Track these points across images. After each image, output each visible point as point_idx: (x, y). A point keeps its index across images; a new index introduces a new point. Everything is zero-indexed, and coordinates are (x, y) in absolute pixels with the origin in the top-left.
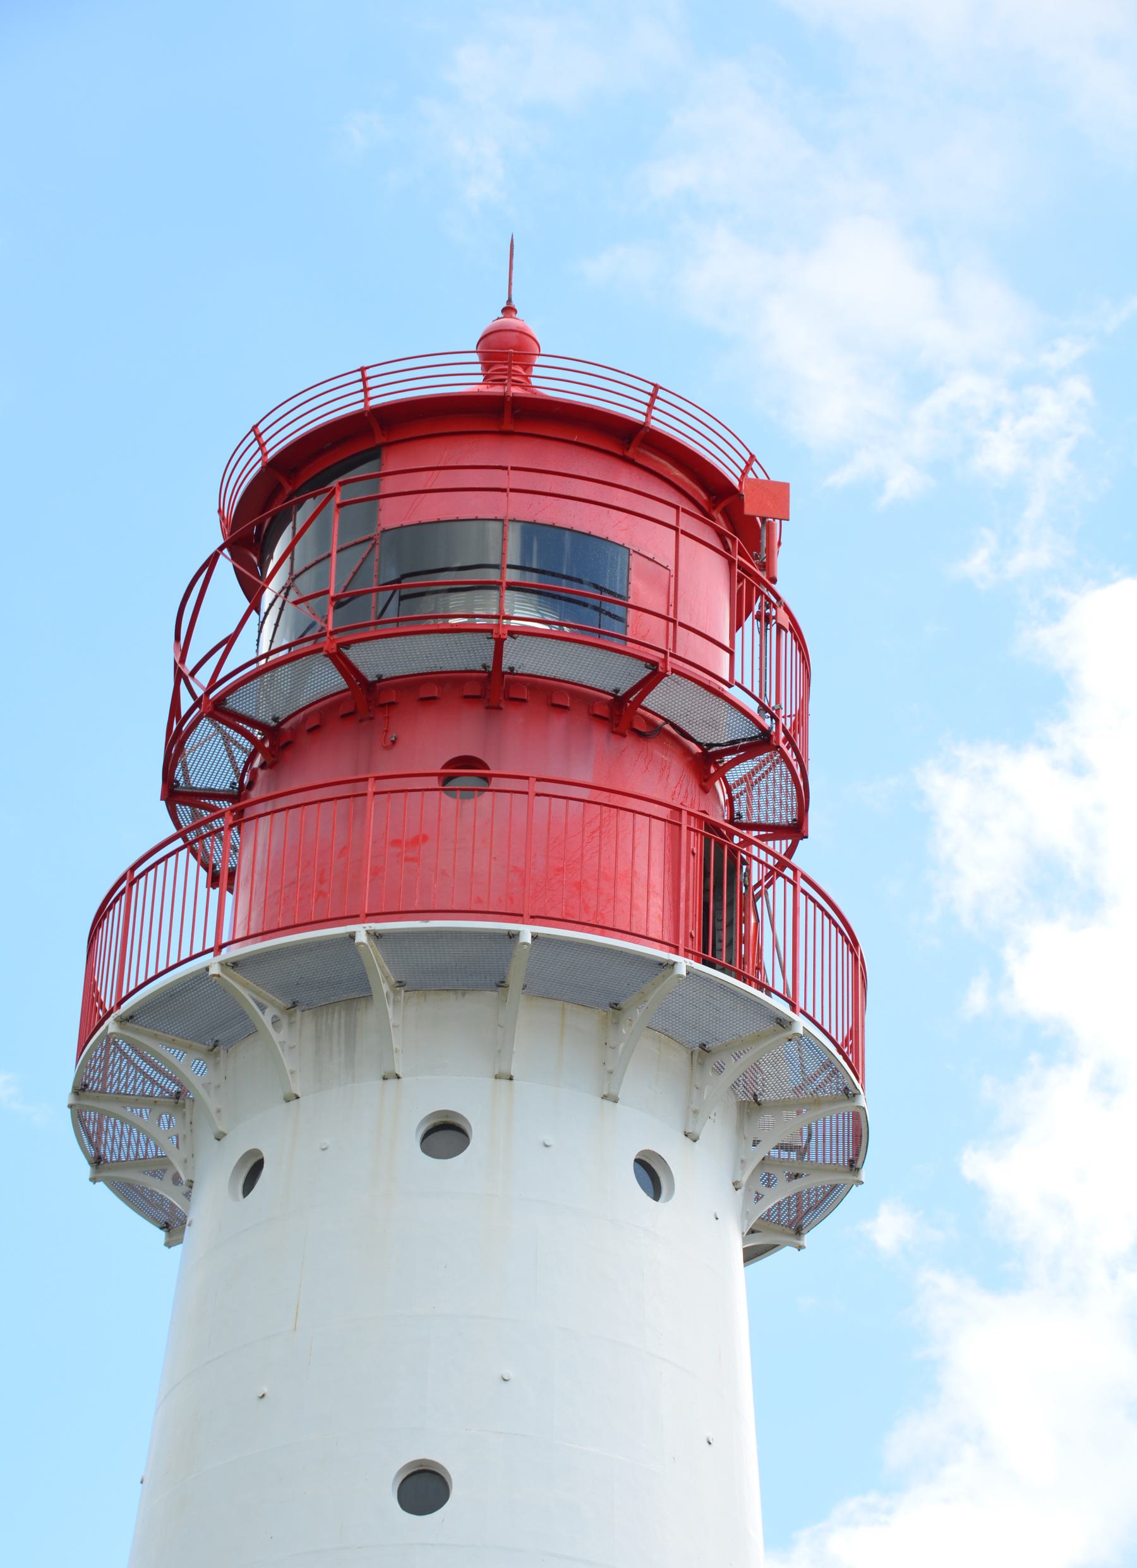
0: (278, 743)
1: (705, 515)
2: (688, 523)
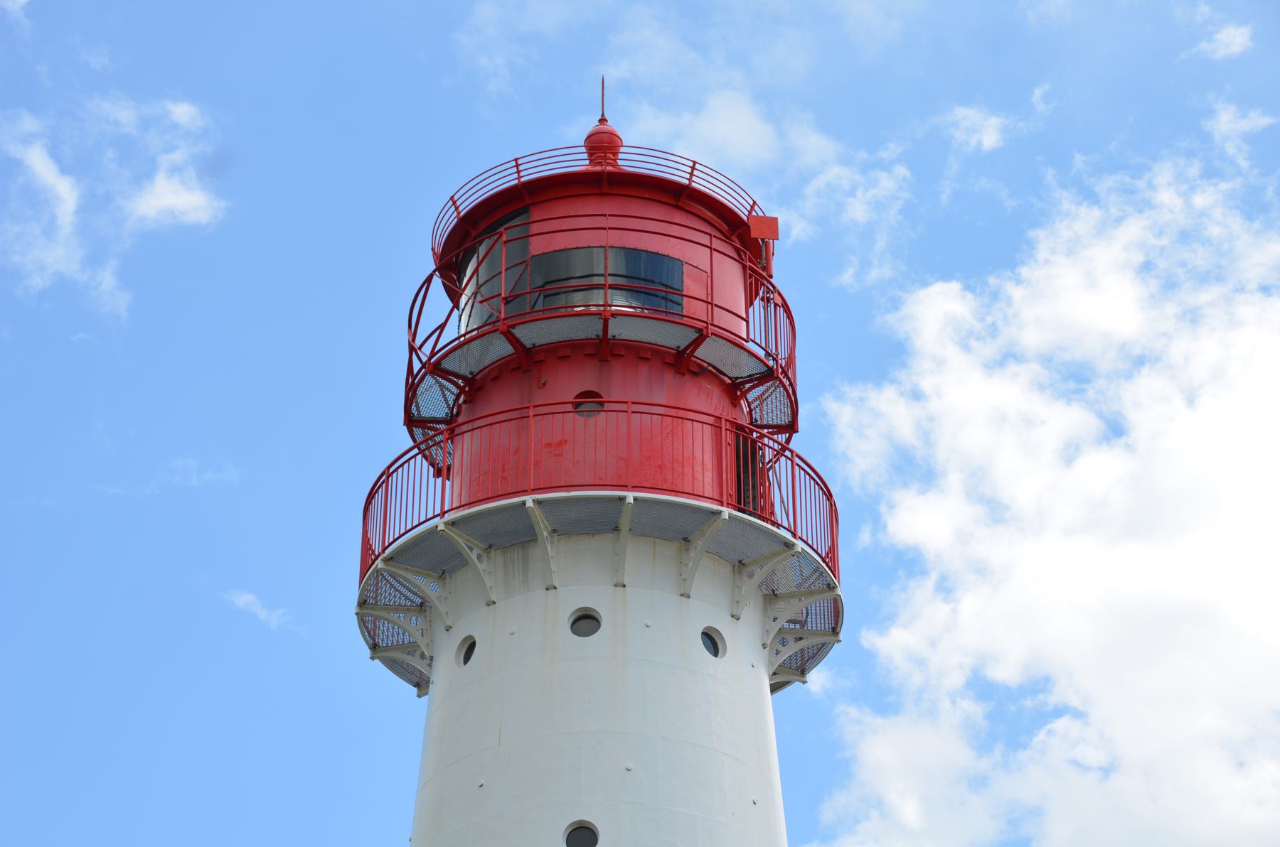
0: (474, 388)
1: (727, 238)
2: (717, 244)
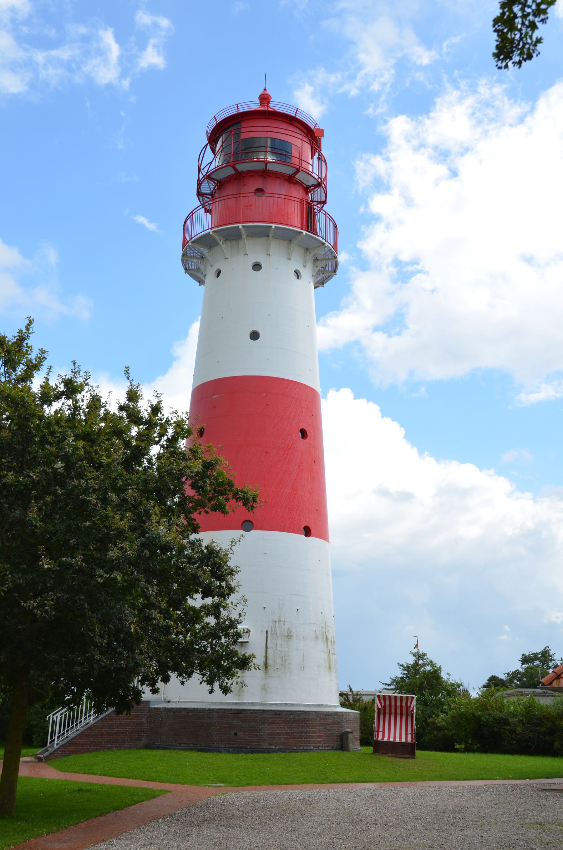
0: (221, 184)
1: (307, 136)
2: (304, 139)
